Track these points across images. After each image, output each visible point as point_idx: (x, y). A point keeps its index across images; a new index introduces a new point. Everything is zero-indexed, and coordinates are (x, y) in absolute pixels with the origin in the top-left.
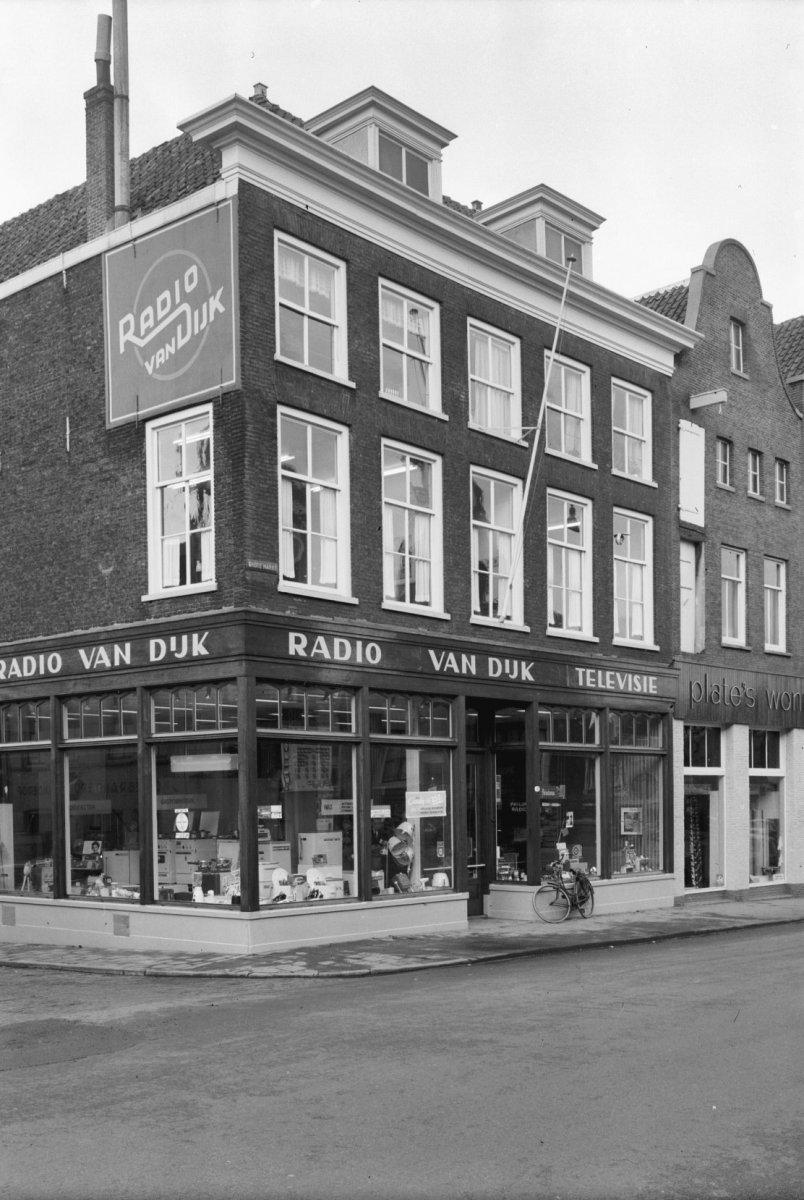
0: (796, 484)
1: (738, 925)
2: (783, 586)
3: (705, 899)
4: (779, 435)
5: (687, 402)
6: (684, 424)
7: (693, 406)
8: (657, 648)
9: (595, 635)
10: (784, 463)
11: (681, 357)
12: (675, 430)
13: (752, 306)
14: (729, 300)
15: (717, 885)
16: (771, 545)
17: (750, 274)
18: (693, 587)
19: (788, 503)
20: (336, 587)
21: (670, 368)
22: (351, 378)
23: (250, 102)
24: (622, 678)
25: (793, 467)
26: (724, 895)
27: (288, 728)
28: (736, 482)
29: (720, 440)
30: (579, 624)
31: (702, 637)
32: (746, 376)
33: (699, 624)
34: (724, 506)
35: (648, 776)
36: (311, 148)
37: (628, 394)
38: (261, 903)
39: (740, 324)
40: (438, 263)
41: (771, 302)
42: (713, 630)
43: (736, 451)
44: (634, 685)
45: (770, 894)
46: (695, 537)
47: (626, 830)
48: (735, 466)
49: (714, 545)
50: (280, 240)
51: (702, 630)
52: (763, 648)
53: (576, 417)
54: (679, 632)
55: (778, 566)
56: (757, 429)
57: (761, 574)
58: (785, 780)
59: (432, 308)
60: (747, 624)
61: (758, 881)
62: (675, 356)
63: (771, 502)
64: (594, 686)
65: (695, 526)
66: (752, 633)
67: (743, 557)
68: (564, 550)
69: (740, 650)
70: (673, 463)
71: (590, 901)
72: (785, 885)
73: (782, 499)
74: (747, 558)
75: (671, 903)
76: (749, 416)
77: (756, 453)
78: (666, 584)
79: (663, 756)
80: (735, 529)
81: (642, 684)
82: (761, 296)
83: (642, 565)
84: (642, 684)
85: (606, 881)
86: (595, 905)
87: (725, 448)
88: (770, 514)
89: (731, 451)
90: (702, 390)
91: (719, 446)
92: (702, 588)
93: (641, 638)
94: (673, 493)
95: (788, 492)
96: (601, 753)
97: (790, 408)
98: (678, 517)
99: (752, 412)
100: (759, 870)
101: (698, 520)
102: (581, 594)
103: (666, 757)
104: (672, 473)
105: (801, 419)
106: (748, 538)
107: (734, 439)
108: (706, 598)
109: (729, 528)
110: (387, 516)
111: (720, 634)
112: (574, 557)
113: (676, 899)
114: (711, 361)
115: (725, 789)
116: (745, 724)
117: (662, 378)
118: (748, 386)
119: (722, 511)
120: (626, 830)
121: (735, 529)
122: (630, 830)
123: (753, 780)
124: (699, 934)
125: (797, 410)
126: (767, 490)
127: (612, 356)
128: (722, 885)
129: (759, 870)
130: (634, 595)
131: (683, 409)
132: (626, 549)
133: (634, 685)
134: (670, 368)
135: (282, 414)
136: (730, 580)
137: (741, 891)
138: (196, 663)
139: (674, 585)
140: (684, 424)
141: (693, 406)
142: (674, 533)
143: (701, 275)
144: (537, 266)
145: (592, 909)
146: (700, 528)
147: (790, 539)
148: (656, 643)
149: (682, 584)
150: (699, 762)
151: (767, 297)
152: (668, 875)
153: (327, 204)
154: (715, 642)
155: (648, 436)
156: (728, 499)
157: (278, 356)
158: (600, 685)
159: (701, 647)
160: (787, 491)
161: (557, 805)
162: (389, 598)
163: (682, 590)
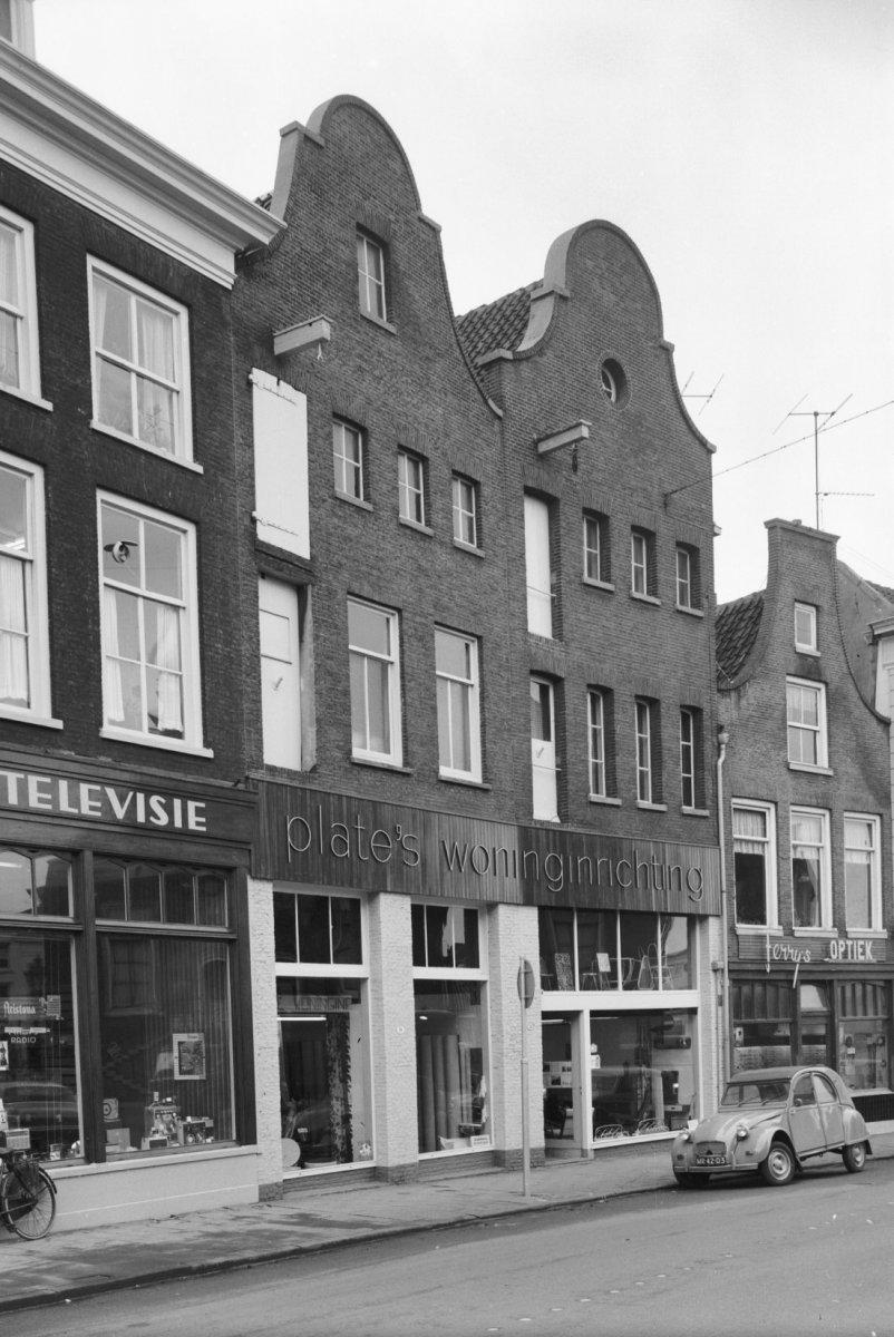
0: (492, 519)
1: (307, 1244)
2: (475, 679)
3: (336, 1183)
4: (457, 436)
5: (268, 342)
6: (258, 376)
7: (278, 350)
8: (209, 753)
9: (56, 715)
10: (471, 484)
11: (249, 259)
12: (243, 384)
13: (401, 218)
14: (354, 196)
15: (361, 1159)
16: (448, 608)
17: (396, 166)
19: (479, 546)
20: (29, 706)
21: (228, 273)
22: (45, 394)
23: (256, 205)
24: (122, 800)
25: (486, 491)
26: (376, 1175)
28: (373, 495)
29: (328, 417)
30: (24, 696)
31: (312, 745)
32: (392, 329)
34: (351, 531)
35: (214, 972)
36: (100, 123)
37: (133, 299)
39: (380, 244)
40: (149, 227)
41: (291, 121)
42: (334, 734)
43: (374, 445)
44: (149, 812)
45: (469, 1168)
46: (302, 578)
47: (181, 1073)
48: (372, 468)
49: (331, 593)
50: (94, 269)
51: (312, 732)
52: (436, 772)
53: (167, 388)
54: (259, 731)
55: (467, 646)
56: (416, 418)
58: (369, 981)
59: (20, 230)
60: (404, 730)
61: (451, 1147)
62: (236, 256)
63: (447, 540)
64: (49, 807)
65: (291, 554)
66: (414, 747)
67: (394, 623)
68: (140, 601)
69: (389, 771)
70: (238, 439)
71: (45, 1206)
72: (492, 1152)
73: (471, 541)
74: (480, 648)
75: (256, 1198)
76: (398, 392)
77: (418, 459)
78: (227, 643)
79: (231, 941)
80: (375, 572)
81: (170, 813)
82: (418, 206)
83: (176, 608)
84: (170, 813)
85: (94, 1167)
86: (57, 1215)
87: (417, 469)
88: (444, 559)
89: (478, 497)
90: (289, 322)
91: (342, 437)
92: (310, 661)
93: (177, 734)
96: (77, 933)
97: (477, 396)
98: (253, 534)
99: (403, 387)
100: (454, 1130)
101: (298, 544)
102: (26, 638)
103: (237, 944)
104: (237, 455)
105: (499, 418)
106: (402, 591)
107: (368, 424)
108: (317, 680)
109: (364, 568)
110: (108, 605)
111: (348, 742)
112: (164, 618)
113: (262, 1189)
114: (318, 286)
115: (370, 1001)
116: (406, 894)
117: (209, 286)
118: (396, 345)
119: (348, 539)
120: (181, 1073)
122: (190, 1072)
123: (422, 987)
124: (205, 1271)
125: (491, 402)
126: (438, 518)
127: (86, 218)
128: (371, 1158)
129: (454, 1130)
131: (258, 351)
132: (137, 569)
133: (149, 812)
134: (228, 273)
135: (102, 501)
136: (371, 658)
137: (403, 1167)
139: (245, 648)
140: (258, 376)
141: (278, 350)
142: (244, 560)
143: (294, 139)
144: (108, 129)
145: (50, 1223)
146: (299, 559)
147: (483, 603)
148: (207, 744)
149: (264, 650)
150: (315, 954)
151: (429, 209)
152: (245, 1149)
153: (43, 159)
154: (338, 754)
155: (183, 382)
156: (357, 518)
157: (96, 424)
158: (64, 807)
159: (310, 761)
160: (477, 528)
161: (43, 1030)
162: (113, 723)
163: (264, 661)
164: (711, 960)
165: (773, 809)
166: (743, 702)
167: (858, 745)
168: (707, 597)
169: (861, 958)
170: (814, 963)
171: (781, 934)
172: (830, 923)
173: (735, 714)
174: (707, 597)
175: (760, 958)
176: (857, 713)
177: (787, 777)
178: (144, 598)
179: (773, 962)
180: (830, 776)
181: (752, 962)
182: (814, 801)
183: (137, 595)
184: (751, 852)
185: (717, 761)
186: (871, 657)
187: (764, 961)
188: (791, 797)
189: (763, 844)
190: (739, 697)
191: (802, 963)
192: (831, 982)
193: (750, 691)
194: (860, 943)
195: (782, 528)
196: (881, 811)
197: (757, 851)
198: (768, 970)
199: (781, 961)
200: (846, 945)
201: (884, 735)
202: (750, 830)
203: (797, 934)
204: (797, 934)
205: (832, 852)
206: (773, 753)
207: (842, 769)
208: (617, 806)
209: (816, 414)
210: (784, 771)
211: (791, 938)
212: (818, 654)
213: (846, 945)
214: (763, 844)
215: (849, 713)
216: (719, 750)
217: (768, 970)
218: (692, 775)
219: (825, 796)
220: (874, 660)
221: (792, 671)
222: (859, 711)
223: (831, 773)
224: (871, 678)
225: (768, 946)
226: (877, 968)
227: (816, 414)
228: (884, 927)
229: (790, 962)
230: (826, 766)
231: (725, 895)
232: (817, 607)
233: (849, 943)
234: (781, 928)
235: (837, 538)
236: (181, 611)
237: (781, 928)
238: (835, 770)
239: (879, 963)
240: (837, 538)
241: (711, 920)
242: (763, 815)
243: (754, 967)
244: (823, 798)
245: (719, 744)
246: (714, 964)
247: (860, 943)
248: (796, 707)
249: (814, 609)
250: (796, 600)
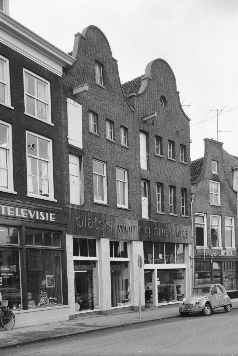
0: (131, 138)
1: (82, 331)
2: (126, 181)
3: (90, 315)
4: (122, 116)
5: (71, 91)
6: (69, 100)
7: (74, 93)
8: (56, 201)
9: (15, 190)
10: (126, 129)
11: (66, 69)
12: (65, 102)
14: (94, 52)
15: (96, 308)
16: (119, 162)
17: (105, 44)
18: (78, 175)
19: (128, 145)
20: (8, 188)
21: (61, 73)
22: (12, 105)
24: (32, 213)
25: (129, 131)
26: (100, 313)
28: (99, 132)
29: (87, 111)
30: (6, 185)
31: (83, 198)
32: (104, 88)
33: (82, 192)
34: (93, 141)
35: (57, 259)
36: (27, 33)
37: (36, 80)
39: (101, 65)
40: (40, 61)
41: (78, 32)
42: (89, 195)
43: (100, 118)
44: (40, 216)
45: (125, 311)
47: (48, 286)
48: (99, 125)
49: (88, 158)
50: (25, 72)
51: (83, 195)
52: (116, 205)
53: (44, 103)
54: (69, 195)
55: (124, 172)
56: (111, 111)
58: (98, 261)
59: (5, 61)
60: (108, 194)
61: (120, 305)
62: (63, 68)
63: (119, 144)
64: (13, 215)
65: (77, 148)
66: (110, 199)
67: (105, 166)
68: (37, 160)
69: (104, 205)
70: (63, 117)
71: (12, 321)
72: (131, 307)
73: (125, 144)
74: (128, 173)
75: (68, 319)
76: (106, 104)
77: (111, 122)
78: (60, 171)
79: (61, 251)
80: (100, 152)
81: (45, 216)
82: (111, 55)
83: (47, 162)
84: (45, 216)
85: (25, 311)
86: (15, 323)
87: (111, 125)
88: (118, 149)
89: (127, 132)
90: (77, 86)
91: (91, 116)
92: (82, 176)
93: (47, 196)
94: (64, 130)
96: (21, 249)
97: (127, 105)
98: (67, 142)
99: (107, 103)
100: (121, 301)
101: (79, 145)
102: (7, 170)
103: (63, 251)
104: (63, 121)
105: (133, 111)
106: (107, 157)
107: (98, 113)
108: (84, 181)
109: (97, 151)
111: (93, 197)
112: (44, 165)
113: (70, 316)
114: (85, 76)
115: (98, 267)
116: (108, 238)
117: (56, 76)
118: (105, 92)
119: (93, 144)
120: (48, 286)
121: (100, 152)
122: (50, 286)
123: (112, 263)
124: (55, 338)
125: (131, 107)
127: (23, 58)
129: (121, 301)
131: (69, 94)
132: (37, 151)
133: (40, 216)
134: (61, 73)
135: (27, 133)
136: (99, 175)
137: (107, 311)
139: (65, 172)
140: (69, 100)
141: (74, 93)
142: (65, 149)
143: (78, 37)
144: (29, 34)
146: (80, 149)
147: (129, 161)
148: (55, 198)
149: (70, 173)
150: (84, 254)
151: (114, 56)
152: (65, 306)
153: (12, 42)
154: (90, 201)
155: (49, 102)
156: (95, 138)
157: (26, 113)
158: (17, 215)
159: (83, 203)
161: (11, 274)
162: (30, 192)
163: (70, 176)
165: (206, 216)
166: (198, 187)
167: (229, 198)
168: (188, 159)
169: (229, 255)
170: (217, 256)
171: (208, 249)
172: (221, 246)
173: (196, 190)
174: (188, 159)
175: (202, 255)
176: (228, 190)
177: (210, 207)
178: (38, 159)
179: (206, 256)
180: (221, 207)
181: (200, 256)
182: (217, 213)
183: (36, 159)
184: (200, 227)
185: (191, 203)
186: (232, 175)
187: (203, 256)
188: (211, 212)
189: (203, 225)
190: (197, 186)
191: (214, 256)
192: (221, 261)
193: (200, 184)
194: (229, 251)
195: (208, 141)
196: (235, 216)
197: (202, 226)
198: (205, 258)
199: (208, 256)
200: (225, 252)
201: (235, 196)
202: (200, 221)
203: (212, 249)
204: (212, 249)
205: (222, 227)
206: (206, 200)
207: (224, 205)
208: (164, 215)
210: (209, 205)
211: (211, 250)
212: (218, 174)
213: (225, 252)
214: (203, 225)
215: (226, 190)
216: (191, 200)
217: (205, 258)
218: (184, 206)
219: (220, 212)
220: (233, 176)
221: (211, 179)
222: (229, 189)
223: (221, 206)
224: (232, 181)
225: (205, 252)
226: (233, 258)
228: (235, 247)
229: (210, 256)
230: (220, 204)
231: (193, 238)
232: (218, 162)
233: (226, 251)
234: (208, 247)
235: (223, 143)
236: (48, 163)
237: (208, 247)
238: (222, 205)
239: (234, 256)
240: (223, 143)
241: (189, 245)
242: (203, 217)
243: (201, 258)
244: (219, 213)
245: (192, 198)
246: (190, 257)
247: (229, 251)
248: (212, 188)
249: (217, 162)
250: (212, 160)
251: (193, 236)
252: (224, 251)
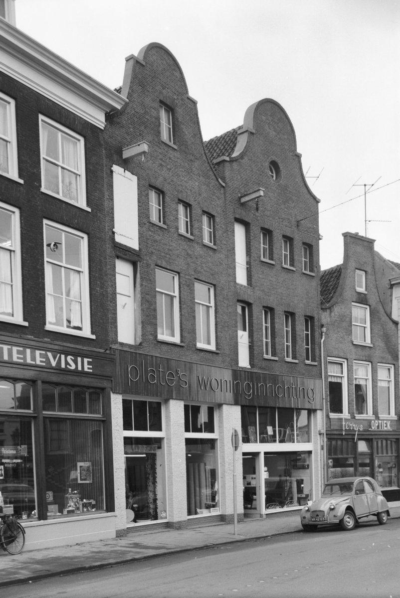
0: (220, 232)
1: (137, 556)
2: (212, 304)
3: (151, 529)
4: (205, 195)
5: (120, 153)
6: (115, 168)
7: (124, 156)
8: (94, 337)
9: (25, 320)
10: (211, 217)
11: (112, 116)
12: (109, 172)
13: (179, 98)
14: (159, 88)
15: (162, 518)
16: (200, 272)
17: (177, 74)
18: (132, 294)
19: (215, 244)
21: (102, 122)
22: (20, 176)
24: (54, 358)
25: (217, 220)
26: (168, 525)
27: (62, 411)
28: (167, 221)
29: (147, 187)
30: (11, 311)
31: (139, 333)
32: (175, 147)
34: (157, 238)
35: (96, 435)
36: (45, 55)
37: (60, 134)
38: (49, 514)
39: (170, 109)
40: (67, 102)
41: (130, 54)
42: (149, 328)
43: (167, 199)
44: (67, 363)
45: (210, 522)
46: (135, 258)
47: (81, 480)
48: (167, 209)
49: (148, 265)
51: (139, 327)
52: (195, 345)
53: (75, 173)
54: (116, 327)
55: (209, 289)
56: (186, 187)
57: (192, 292)
58: (165, 439)
59: (9, 103)
60: (181, 327)
61: (202, 513)
62: (106, 114)
64: (22, 361)
65: (130, 248)
66: (185, 334)
67: (176, 278)
68: (63, 269)
69: (174, 345)
70: (106, 197)
71: (20, 539)
72: (220, 515)
73: (211, 242)
74: (215, 290)
75: (114, 536)
77: (187, 205)
78: (102, 288)
79: (103, 421)
80: (168, 256)
81: (76, 364)
82: (187, 92)
83: (79, 272)
84: (76, 364)
85: (42, 522)
86: (26, 543)
87: (186, 210)
88: (199, 250)
89: (214, 222)
90: (129, 144)
91: (153, 196)
92: (139, 296)
93: (79, 329)
95: (164, 217)
96: (35, 417)
97: (214, 177)
98: (113, 239)
99: (180, 173)
100: (203, 505)
101: (133, 243)
102: (12, 286)
103: (106, 422)
104: (106, 203)
105: (223, 187)
106: (180, 264)
107: (165, 190)
108: (142, 304)
109: (163, 254)
111: (156, 332)
112: (74, 277)
113: (117, 532)
114: (142, 128)
115: (166, 448)
116: (182, 400)
117: (94, 128)
118: (177, 154)
119: (156, 241)
120: (81, 480)
122: (85, 480)
123: (189, 442)
124: (92, 569)
125: (220, 180)
127: (38, 97)
128: (166, 518)
129: (203, 505)
130: (72, 293)
131: (115, 157)
132: (61, 254)
133: (67, 363)
134: (102, 122)
136: (166, 294)
137: (180, 522)
138: (105, 378)
139: (110, 290)
140: (115, 168)
141: (124, 156)
142: (109, 250)
143: (131, 62)
144: (48, 58)
146: (134, 250)
147: (216, 270)
148: (93, 333)
149: (118, 291)
150: (141, 427)
151: (192, 94)
152: (110, 514)
153: (19, 71)
154: (151, 337)
155: (82, 171)
156: (160, 232)
158: (29, 361)
159: (139, 341)
161: (19, 461)
162: (50, 323)
163: (118, 296)
164: (318, 429)
165: (346, 362)
166: (333, 314)
167: (384, 333)
168: (316, 267)
169: (385, 428)
170: (364, 431)
171: (349, 418)
172: (372, 413)
173: (329, 319)
174: (316, 267)
176: (383, 319)
177: (352, 348)
178: (65, 267)
179: (346, 430)
180: (371, 347)
181: (337, 430)
182: (364, 358)
183: (61, 266)
184: (336, 381)
185: (321, 340)
186: (390, 294)
187: (342, 430)
188: (354, 357)
189: (341, 377)
190: (331, 312)
191: (359, 431)
192: (372, 439)
193: (336, 309)
194: (385, 422)
195: (350, 236)
196: (394, 363)
197: (339, 380)
198: (344, 434)
199: (349, 430)
200: (379, 423)
201: (396, 329)
202: (335, 371)
203: (356, 418)
204: (356, 418)
205: (372, 381)
206: (346, 337)
207: (377, 344)
208: (276, 361)
209: (365, 185)
210: (351, 345)
211: (354, 419)
212: (366, 293)
213: (379, 423)
214: (341, 377)
215: (380, 319)
216: (322, 335)
217: (344, 434)
218: (310, 347)
219: (369, 356)
220: (391, 295)
221: (354, 300)
222: (385, 318)
223: (372, 346)
224: (390, 303)
225: (344, 423)
226: (392, 433)
227: (365, 185)
228: (395, 415)
229: (354, 430)
230: (370, 342)
232: (366, 272)
233: (380, 422)
234: (350, 415)
235: (375, 241)
236: (81, 273)
237: (350, 415)
238: (374, 344)
239: (393, 431)
240: (375, 241)
241: (318, 411)
242: (341, 364)
243: (337, 433)
244: (368, 357)
245: (322, 333)
246: (319, 431)
247: (385, 422)
248: (356, 316)
249: (364, 273)
250: (356, 269)
251: (324, 397)
252: (376, 421)
